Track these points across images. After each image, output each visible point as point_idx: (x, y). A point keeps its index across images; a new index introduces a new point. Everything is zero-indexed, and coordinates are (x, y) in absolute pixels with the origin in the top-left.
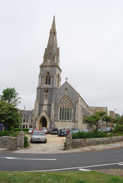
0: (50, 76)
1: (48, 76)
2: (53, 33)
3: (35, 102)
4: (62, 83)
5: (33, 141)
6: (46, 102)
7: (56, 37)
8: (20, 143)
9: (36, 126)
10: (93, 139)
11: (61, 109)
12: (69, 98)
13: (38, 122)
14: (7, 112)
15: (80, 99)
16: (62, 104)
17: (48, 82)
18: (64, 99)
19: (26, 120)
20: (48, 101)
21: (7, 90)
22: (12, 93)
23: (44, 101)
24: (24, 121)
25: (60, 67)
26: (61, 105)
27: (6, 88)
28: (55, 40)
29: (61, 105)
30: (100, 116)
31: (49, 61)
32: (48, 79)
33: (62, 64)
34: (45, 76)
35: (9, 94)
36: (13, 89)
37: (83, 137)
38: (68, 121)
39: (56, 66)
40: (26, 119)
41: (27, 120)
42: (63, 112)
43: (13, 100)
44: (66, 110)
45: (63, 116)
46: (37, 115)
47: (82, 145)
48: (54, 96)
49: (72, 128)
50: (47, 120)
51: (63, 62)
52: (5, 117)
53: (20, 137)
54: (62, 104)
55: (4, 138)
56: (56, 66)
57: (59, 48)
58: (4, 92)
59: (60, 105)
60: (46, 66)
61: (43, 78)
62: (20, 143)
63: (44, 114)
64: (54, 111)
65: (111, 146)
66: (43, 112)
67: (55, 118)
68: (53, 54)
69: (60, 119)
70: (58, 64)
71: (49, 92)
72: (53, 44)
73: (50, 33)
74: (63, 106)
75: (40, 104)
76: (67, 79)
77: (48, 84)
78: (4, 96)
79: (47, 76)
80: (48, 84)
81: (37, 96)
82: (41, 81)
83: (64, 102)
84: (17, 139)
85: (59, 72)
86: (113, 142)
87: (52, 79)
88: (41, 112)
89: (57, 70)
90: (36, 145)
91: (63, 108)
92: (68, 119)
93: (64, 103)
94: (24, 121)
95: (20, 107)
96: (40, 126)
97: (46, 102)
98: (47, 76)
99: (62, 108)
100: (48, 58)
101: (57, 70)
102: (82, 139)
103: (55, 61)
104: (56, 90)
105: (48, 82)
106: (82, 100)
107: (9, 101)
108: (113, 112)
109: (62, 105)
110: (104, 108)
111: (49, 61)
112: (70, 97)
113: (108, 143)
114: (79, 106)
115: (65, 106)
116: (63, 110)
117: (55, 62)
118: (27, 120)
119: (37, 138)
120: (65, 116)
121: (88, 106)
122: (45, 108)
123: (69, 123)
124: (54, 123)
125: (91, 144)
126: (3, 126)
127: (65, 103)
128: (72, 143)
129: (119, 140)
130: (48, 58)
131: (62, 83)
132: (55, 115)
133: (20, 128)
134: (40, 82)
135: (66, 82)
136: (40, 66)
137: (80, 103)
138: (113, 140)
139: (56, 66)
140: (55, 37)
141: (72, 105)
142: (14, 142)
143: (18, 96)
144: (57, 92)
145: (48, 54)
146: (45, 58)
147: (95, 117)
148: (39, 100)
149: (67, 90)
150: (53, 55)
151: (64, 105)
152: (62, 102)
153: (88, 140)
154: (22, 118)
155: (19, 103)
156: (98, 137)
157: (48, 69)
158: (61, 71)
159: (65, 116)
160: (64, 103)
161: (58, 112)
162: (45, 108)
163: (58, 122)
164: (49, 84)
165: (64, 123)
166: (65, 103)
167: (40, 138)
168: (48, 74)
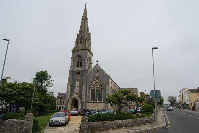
0: (81, 59)
1: (80, 59)
2: (85, 19)
3: (67, 84)
4: (93, 65)
5: (51, 124)
6: (77, 84)
8: (27, 127)
9: (68, 108)
10: (114, 121)
11: (92, 90)
12: (100, 80)
13: (70, 103)
14: (19, 92)
15: (110, 80)
16: (93, 86)
17: (80, 64)
18: (95, 81)
19: (62, 102)
20: (80, 83)
21: (40, 72)
22: (45, 76)
23: (75, 83)
24: (61, 103)
25: (92, 50)
27: (38, 71)
28: (86, 26)
30: (122, 94)
31: (80, 45)
33: (93, 48)
34: (77, 60)
35: (42, 77)
36: (46, 72)
37: (101, 120)
38: (99, 102)
39: (88, 50)
40: (62, 101)
41: (63, 102)
42: (94, 94)
43: (45, 82)
44: (99, 91)
45: (94, 97)
46: (69, 97)
47: (100, 129)
48: (85, 78)
49: (103, 109)
50: (78, 102)
51: (95, 46)
52: (15, 97)
53: (27, 120)
54: (93, 86)
55: (10, 121)
56: (87, 50)
57: (90, 33)
58: (37, 75)
60: (77, 50)
61: (75, 61)
62: (27, 127)
63: (75, 96)
64: (85, 93)
65: (134, 130)
66: (75, 94)
68: (85, 38)
69: (91, 100)
70: (90, 48)
71: (81, 74)
72: (84, 30)
73: (82, 19)
75: (71, 85)
76: (97, 61)
77: (79, 67)
78: (36, 79)
79: (79, 59)
80: (79, 67)
81: (69, 78)
82: (73, 64)
84: (23, 123)
85: (90, 55)
86: (138, 125)
87: (83, 62)
88: (73, 93)
89: (88, 53)
90: (51, 129)
91: (94, 89)
92: (99, 100)
93: (95, 84)
94: (61, 103)
95: (49, 90)
97: (77, 84)
98: (79, 59)
99: (93, 89)
100: (80, 42)
101: (88, 53)
102: (100, 122)
103: (87, 45)
104: (87, 72)
105: (80, 64)
106: (113, 82)
107: (42, 83)
108: (143, 93)
111: (80, 45)
112: (100, 79)
113: (133, 126)
114: (110, 87)
115: (96, 87)
116: (94, 91)
117: (86, 46)
118: (63, 102)
119: (54, 120)
120: (96, 98)
121: (119, 88)
122: (77, 90)
123: (100, 104)
124: (86, 104)
125: (111, 128)
126: (15, 108)
127: (96, 84)
128: (89, 126)
130: (80, 42)
131: (93, 65)
132: (86, 97)
133: (57, 110)
135: (97, 65)
137: (110, 85)
138: (137, 122)
139: (87, 50)
140: (86, 23)
141: (103, 86)
142: (20, 127)
143: (51, 79)
144: (89, 74)
145: (80, 38)
146: (77, 41)
147: (117, 96)
148: (71, 82)
149: (97, 72)
150: (85, 39)
152: (93, 84)
153: (107, 123)
154: (59, 101)
155: (51, 85)
156: (120, 119)
157: (80, 52)
158: (93, 55)
159: (96, 98)
160: (95, 84)
161: (90, 93)
162: (77, 90)
163: (89, 103)
164: (81, 67)
165: (95, 105)
166: (96, 84)
167: (59, 121)
168: (80, 57)
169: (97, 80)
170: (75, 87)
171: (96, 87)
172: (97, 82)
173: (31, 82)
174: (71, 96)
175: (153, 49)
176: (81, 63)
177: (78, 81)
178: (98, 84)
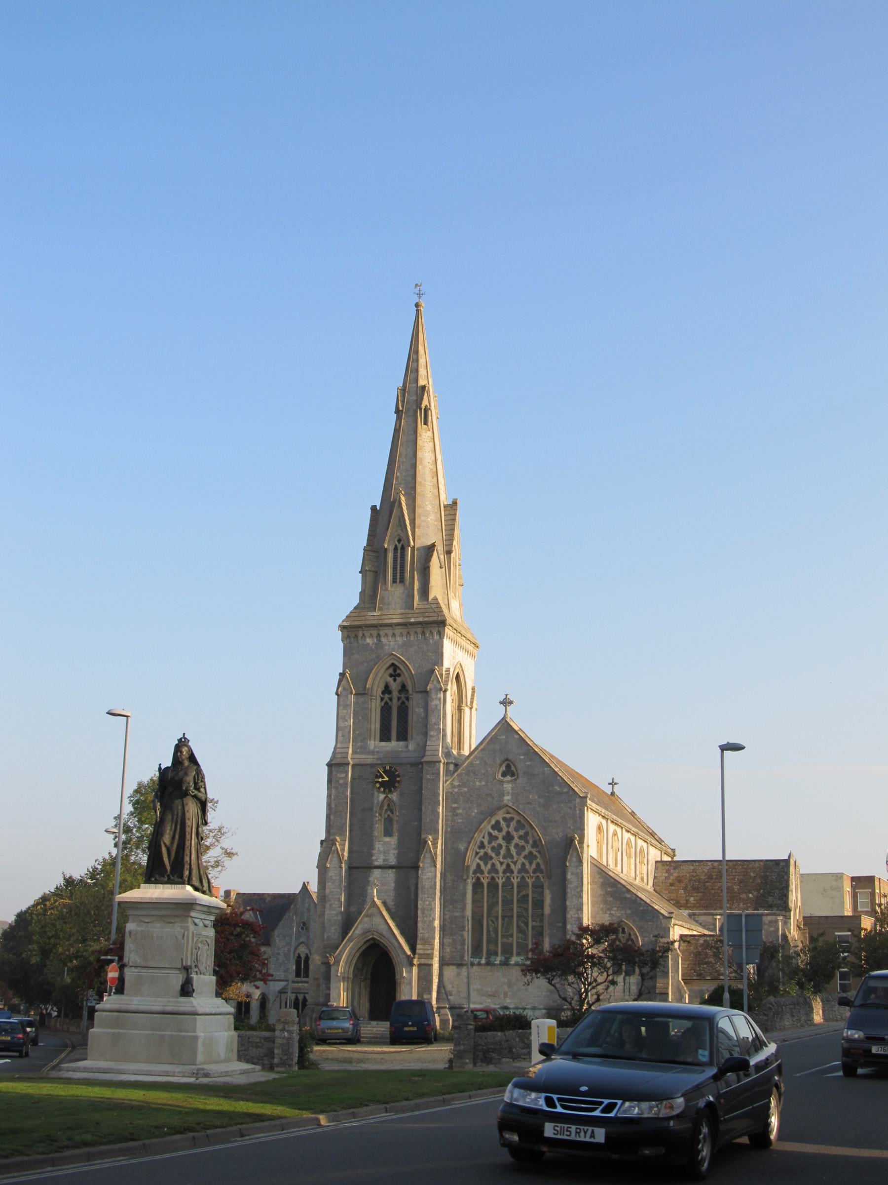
0: (403, 688)
1: (394, 686)
6: (404, 1041)
11: (477, 885)
21: (372, 506)
26: (478, 865)
29: (478, 865)
60: (375, 626)
73: (398, 412)
74: (494, 869)
80: (429, 962)
87: (416, 710)
109: (486, 864)
111: (393, 593)
115: (501, 869)
127: (503, 852)
135: (504, 726)
151: (498, 866)
152: (482, 846)
164: (403, 736)
166: (503, 852)
169: (508, 821)
170: (371, 867)
171: (501, 869)
172: (508, 838)
173: (146, 783)
174: (347, 924)
177: (388, 833)
178: (513, 851)
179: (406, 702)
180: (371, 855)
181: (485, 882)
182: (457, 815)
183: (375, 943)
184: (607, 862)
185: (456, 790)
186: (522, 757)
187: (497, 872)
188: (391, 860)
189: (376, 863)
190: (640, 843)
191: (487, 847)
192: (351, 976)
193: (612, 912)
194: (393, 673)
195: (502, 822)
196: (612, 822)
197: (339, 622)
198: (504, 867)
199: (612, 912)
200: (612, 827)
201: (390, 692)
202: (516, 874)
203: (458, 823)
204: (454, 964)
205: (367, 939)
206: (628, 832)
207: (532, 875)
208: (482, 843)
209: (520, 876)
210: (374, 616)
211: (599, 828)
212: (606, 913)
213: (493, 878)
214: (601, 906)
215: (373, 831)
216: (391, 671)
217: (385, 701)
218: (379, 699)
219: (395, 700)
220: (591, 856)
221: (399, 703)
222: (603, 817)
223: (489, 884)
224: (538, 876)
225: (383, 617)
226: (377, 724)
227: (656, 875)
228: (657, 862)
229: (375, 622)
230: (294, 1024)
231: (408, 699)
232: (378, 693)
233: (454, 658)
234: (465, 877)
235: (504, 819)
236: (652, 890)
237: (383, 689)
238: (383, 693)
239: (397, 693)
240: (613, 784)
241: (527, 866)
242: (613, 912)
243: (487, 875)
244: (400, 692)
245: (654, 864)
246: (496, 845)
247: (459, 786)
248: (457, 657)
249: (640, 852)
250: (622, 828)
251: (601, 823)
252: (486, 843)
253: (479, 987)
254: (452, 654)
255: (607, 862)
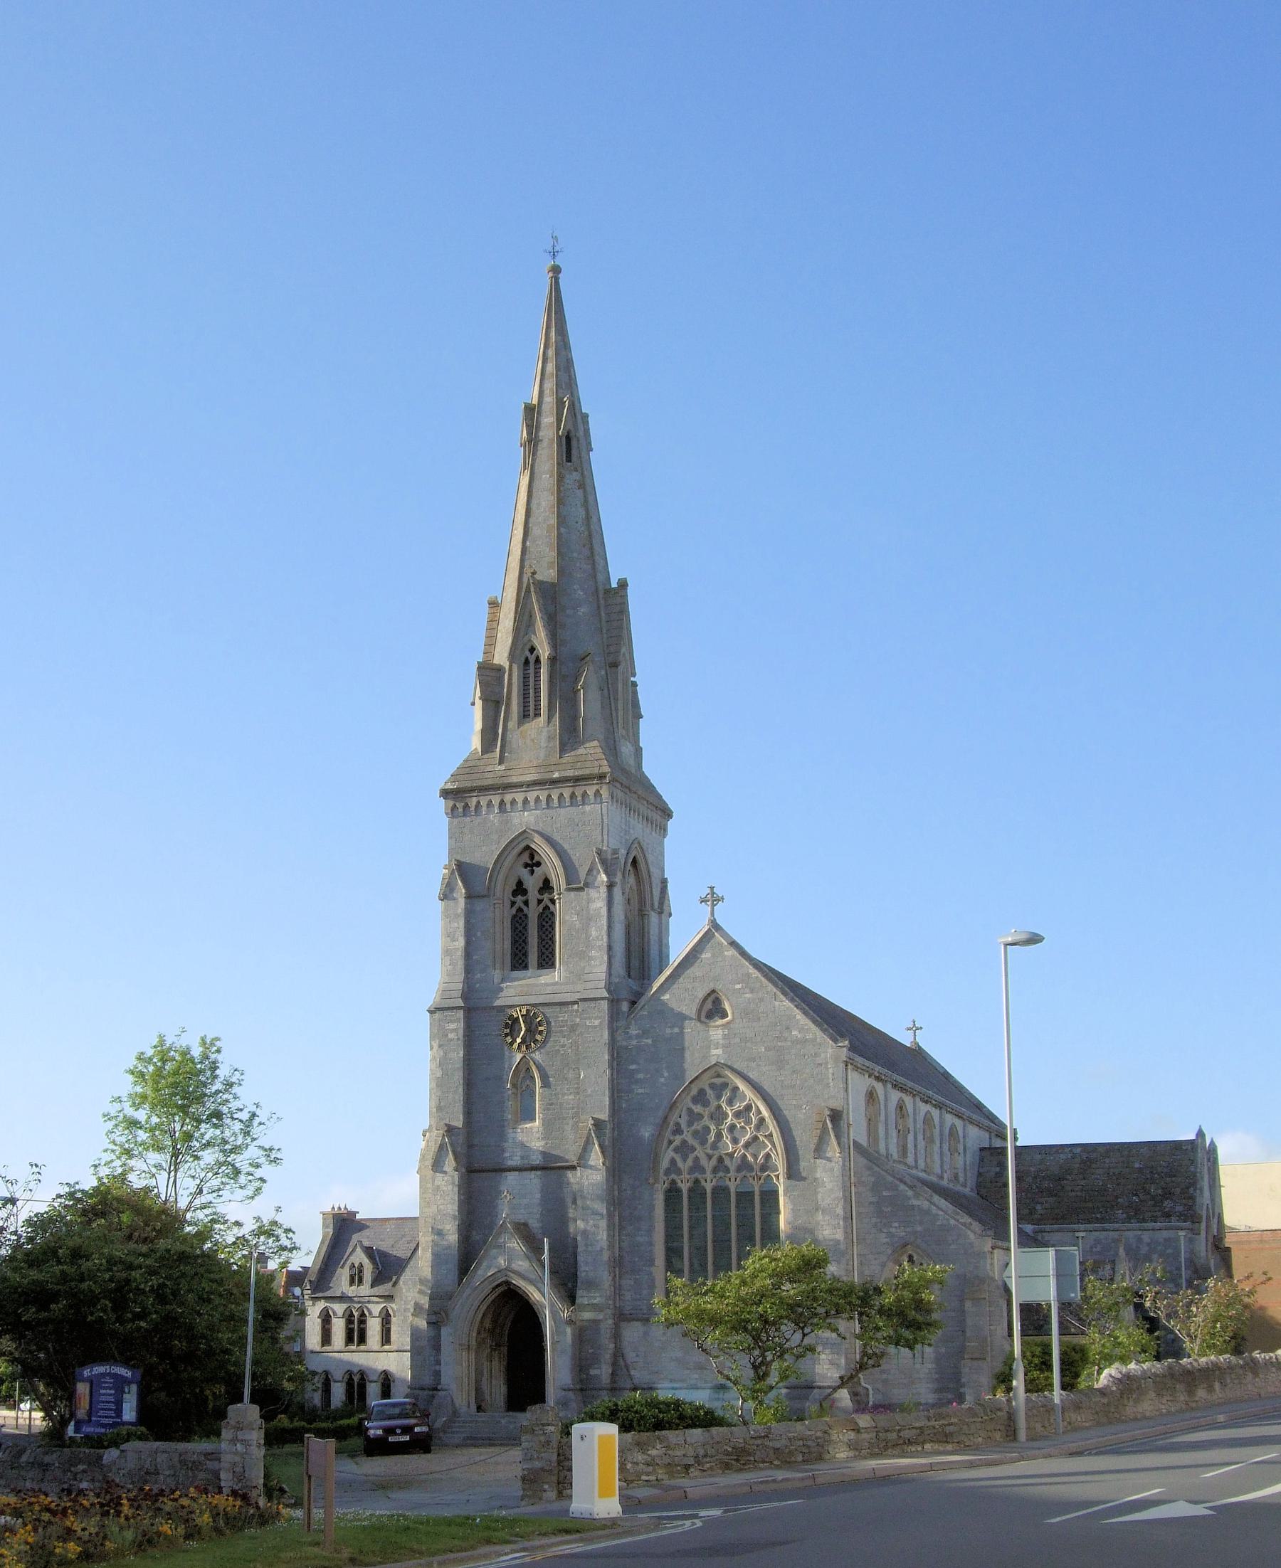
7: (585, 504)
11: (673, 1194)
17: (532, 691)
19: (374, 1327)
24: (356, 1334)
26: (673, 1162)
29: (673, 1162)
32: (533, 912)
34: (503, 890)
40: (376, 1309)
41: (386, 1319)
54: (684, 1149)
59: (665, 1164)
67: (618, 1290)
74: (697, 1167)
76: (713, 899)
80: (533, 957)
83: (697, 1126)
91: (697, 1191)
96: (479, 1373)
99: (709, 1187)
109: (685, 1159)
110: (324, 1219)
115: (709, 1165)
118: (386, 1319)
124: (617, 1336)
125: (687, 1467)
129: (906, 1434)
134: (461, 942)
136: (445, 793)
151: (704, 1161)
152: (678, 1131)
158: (667, 814)
161: (651, 1230)
175: (1006, 945)
176: (547, 920)
179: (525, 908)
180: (503, 1151)
181: (684, 1187)
182: (637, 1081)
183: (509, 1288)
184: (887, 1149)
185: (634, 1042)
186: (738, 986)
187: (703, 1170)
188: (534, 1157)
189: (510, 1163)
190: (949, 1119)
191: (685, 1133)
192: (474, 1342)
193: (891, 1230)
194: (529, 862)
195: (709, 1092)
196: (895, 1086)
197: (442, 785)
198: (714, 1162)
199: (891, 1230)
200: (895, 1096)
201: (524, 892)
202: (732, 1174)
203: (638, 1094)
204: (638, 1320)
205: (497, 1283)
206: (926, 1102)
207: (759, 1174)
208: (678, 1124)
209: (741, 1175)
210: (494, 770)
211: (871, 1096)
212: (881, 1231)
213: (697, 1181)
214: (874, 1220)
215: (504, 1111)
216: (525, 858)
217: (516, 906)
218: (508, 904)
219: (533, 903)
220: (854, 1142)
221: (514, 911)
222: (878, 1079)
223: (690, 1190)
224: (673, 1180)
225: (511, 772)
226: (505, 943)
227: (981, 1170)
228: (982, 1149)
229: (497, 781)
230: (253, 1429)
231: (553, 901)
232: (506, 895)
233: (627, 832)
234: (651, 1181)
235: (712, 1086)
236: (974, 1194)
237: (515, 888)
238: (515, 893)
239: (536, 892)
240: (915, 1028)
241: (680, 1164)
242: (893, 1230)
243: (688, 1177)
244: (541, 891)
245: (978, 1153)
246: (699, 1128)
247: (638, 1036)
248: (632, 831)
249: (951, 1134)
250: (914, 1095)
251: (873, 1087)
252: (683, 1126)
253: (679, 1354)
254: (623, 827)
255: (887, 1149)
